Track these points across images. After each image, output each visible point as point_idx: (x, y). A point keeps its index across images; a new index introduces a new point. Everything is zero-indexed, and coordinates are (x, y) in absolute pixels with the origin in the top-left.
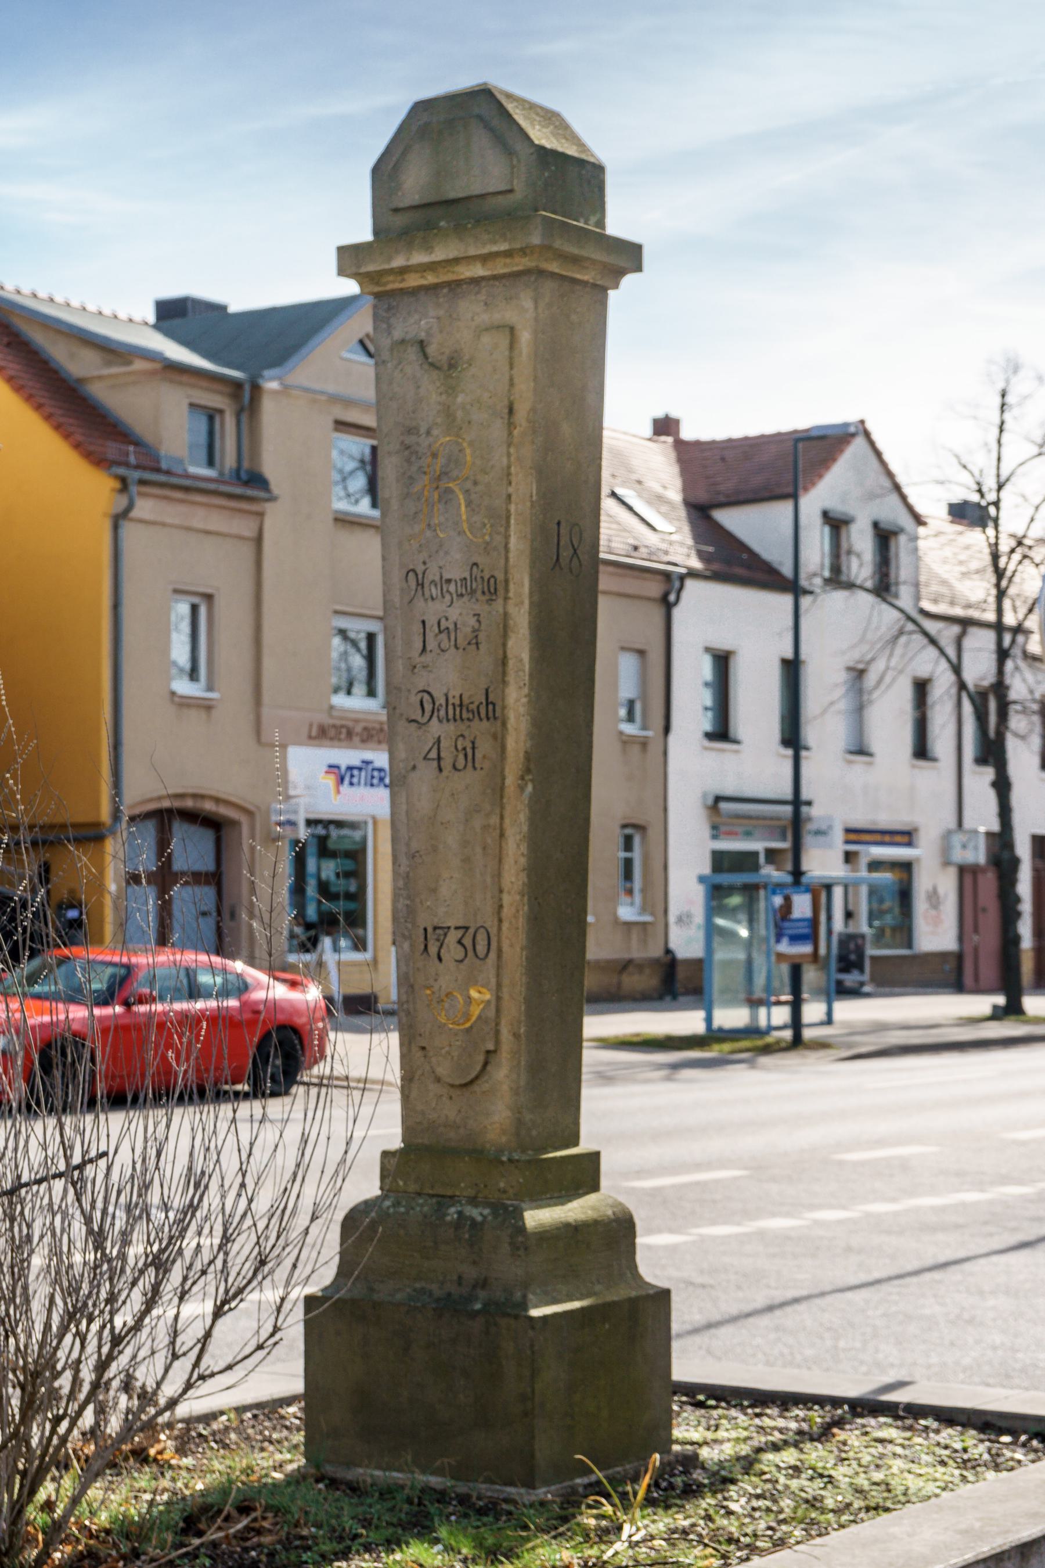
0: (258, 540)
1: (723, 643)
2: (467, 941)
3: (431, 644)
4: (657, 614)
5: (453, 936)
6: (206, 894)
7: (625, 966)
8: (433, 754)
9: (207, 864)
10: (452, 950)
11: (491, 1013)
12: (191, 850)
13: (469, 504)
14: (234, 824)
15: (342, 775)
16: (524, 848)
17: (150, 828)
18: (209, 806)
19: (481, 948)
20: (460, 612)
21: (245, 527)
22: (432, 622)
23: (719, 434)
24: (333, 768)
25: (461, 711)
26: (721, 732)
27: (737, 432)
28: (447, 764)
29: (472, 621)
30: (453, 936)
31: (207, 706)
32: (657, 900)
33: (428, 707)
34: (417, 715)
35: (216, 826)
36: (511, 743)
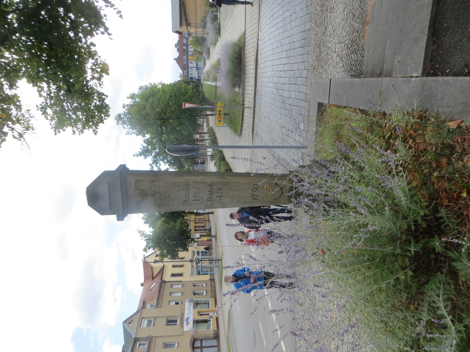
0: (156, 337)
1: (170, 275)
2: (255, 189)
3: (198, 198)
4: (166, 283)
5: (254, 193)
6: (204, 341)
7: (211, 285)
8: (219, 198)
9: (200, 341)
10: (256, 193)
11: (268, 184)
12: (198, 344)
13: (171, 191)
14: (194, 338)
15: (188, 324)
16: (238, 178)
17: (195, 350)
18: (192, 342)
19: (256, 187)
20: (192, 192)
21: (154, 339)
22: (193, 199)
23: (144, 279)
24: (187, 325)
25: (211, 192)
26: (181, 275)
27: (143, 269)
28: (221, 195)
29: (194, 189)
30: (254, 193)
31: (178, 343)
32: (203, 281)
33: (210, 199)
34: (212, 201)
35: (194, 340)
36: (217, 181)
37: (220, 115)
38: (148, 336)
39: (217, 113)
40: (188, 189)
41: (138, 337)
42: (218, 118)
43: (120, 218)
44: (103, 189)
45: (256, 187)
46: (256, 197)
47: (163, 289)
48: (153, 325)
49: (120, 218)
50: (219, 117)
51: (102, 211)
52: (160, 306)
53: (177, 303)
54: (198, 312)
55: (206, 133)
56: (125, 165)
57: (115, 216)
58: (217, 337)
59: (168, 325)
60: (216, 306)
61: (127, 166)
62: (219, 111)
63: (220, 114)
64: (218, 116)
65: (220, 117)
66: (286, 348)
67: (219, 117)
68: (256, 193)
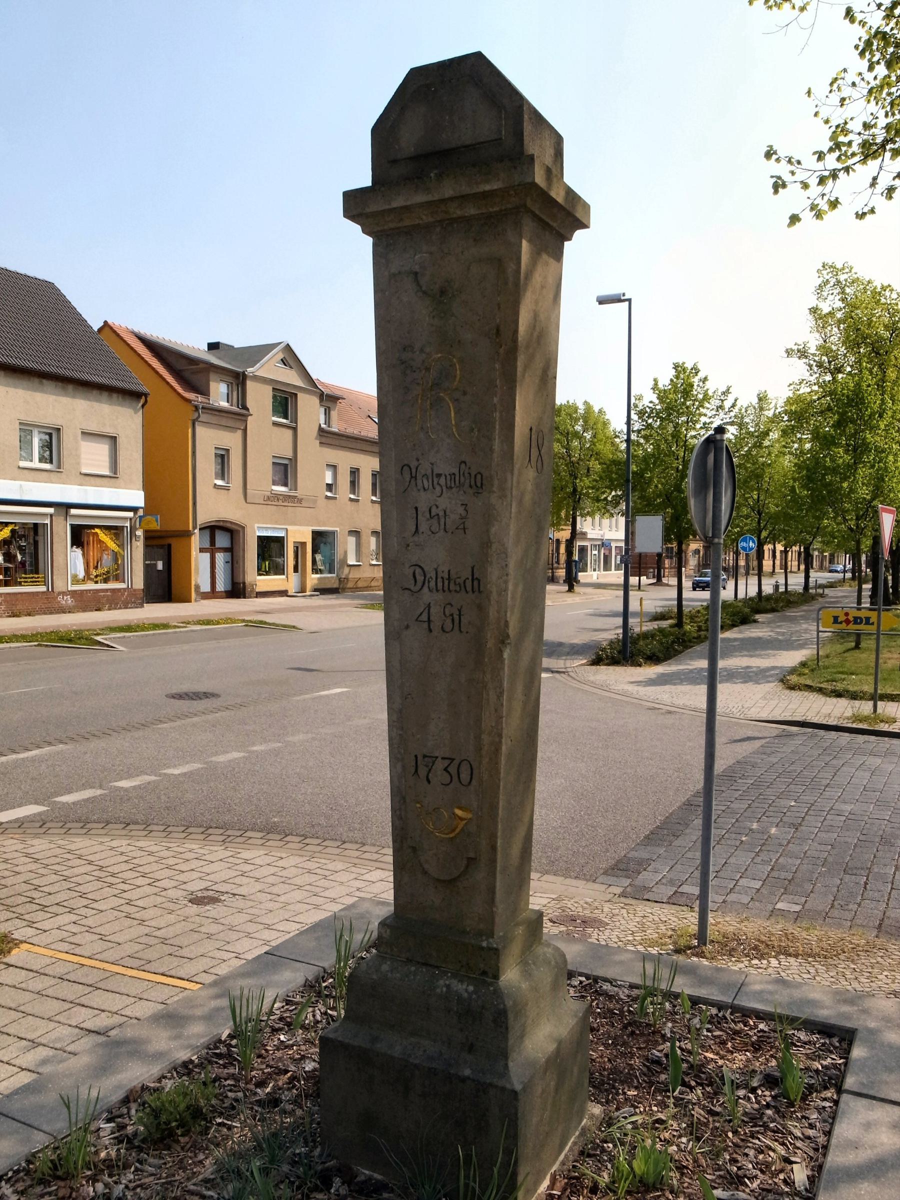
2: (453, 770)
5: (440, 765)
8: (424, 617)
10: (439, 774)
14: (238, 531)
18: (228, 525)
19: (465, 776)
22: (423, 507)
28: (436, 625)
29: (461, 510)
30: (440, 765)
33: (420, 578)
37: (855, 622)
38: (248, 409)
39: (863, 614)
40: (461, 485)
41: (249, 384)
42: (847, 614)
43: (356, 205)
44: (475, 124)
45: (465, 776)
46: (423, 772)
47: (337, 442)
48: (275, 424)
49: (356, 205)
50: (851, 618)
51: (384, 132)
52: (324, 440)
53: (329, 487)
54: (304, 544)
55: (807, 577)
56: (585, 226)
57: (367, 182)
58: (237, 590)
59: (228, 450)
60: (315, 590)
61: (579, 234)
62: (868, 619)
63: (857, 621)
64: (854, 613)
65: (848, 622)
66: (126, 790)
67: (851, 618)
68: (439, 774)
